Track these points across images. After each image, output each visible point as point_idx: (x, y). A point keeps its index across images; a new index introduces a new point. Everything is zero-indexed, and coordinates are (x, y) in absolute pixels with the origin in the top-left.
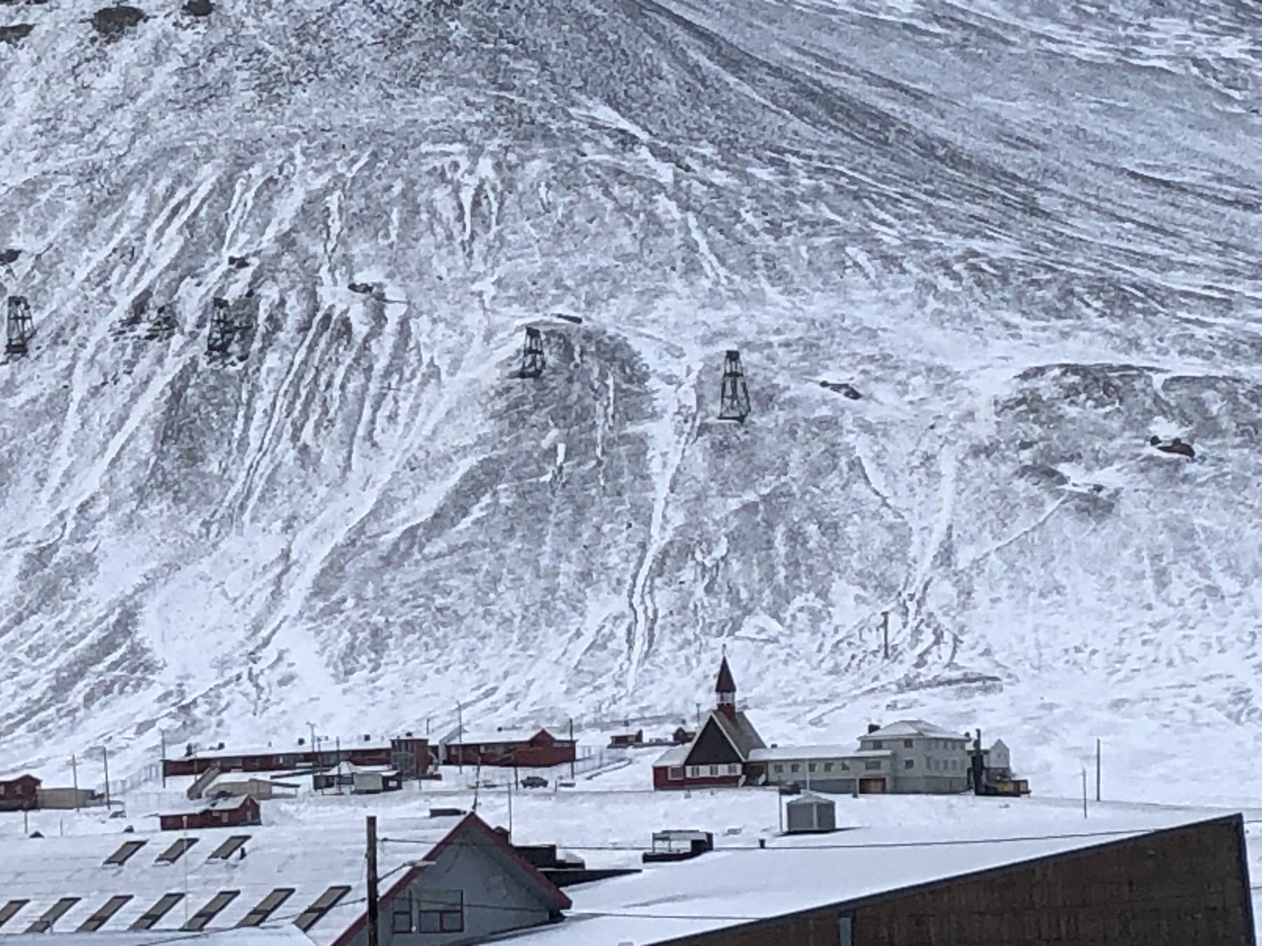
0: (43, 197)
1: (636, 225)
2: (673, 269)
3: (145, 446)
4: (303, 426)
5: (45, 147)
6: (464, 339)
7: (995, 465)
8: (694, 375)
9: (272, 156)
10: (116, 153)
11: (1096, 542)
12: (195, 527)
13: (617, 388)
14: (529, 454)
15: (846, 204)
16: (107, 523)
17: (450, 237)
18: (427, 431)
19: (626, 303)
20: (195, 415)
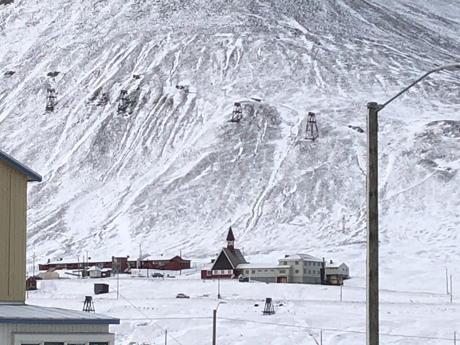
0: (72, 52)
1: (292, 65)
2: (304, 82)
3: (87, 146)
4: (147, 139)
5: (77, 34)
6: (215, 107)
7: (410, 159)
8: (300, 122)
9: (159, 37)
10: (102, 36)
11: (443, 191)
12: (98, 177)
13: (268, 127)
14: (228, 151)
15: (382, 58)
16: (67, 175)
17: (219, 69)
18: (193, 142)
19: (281, 94)
20: (108, 135)
